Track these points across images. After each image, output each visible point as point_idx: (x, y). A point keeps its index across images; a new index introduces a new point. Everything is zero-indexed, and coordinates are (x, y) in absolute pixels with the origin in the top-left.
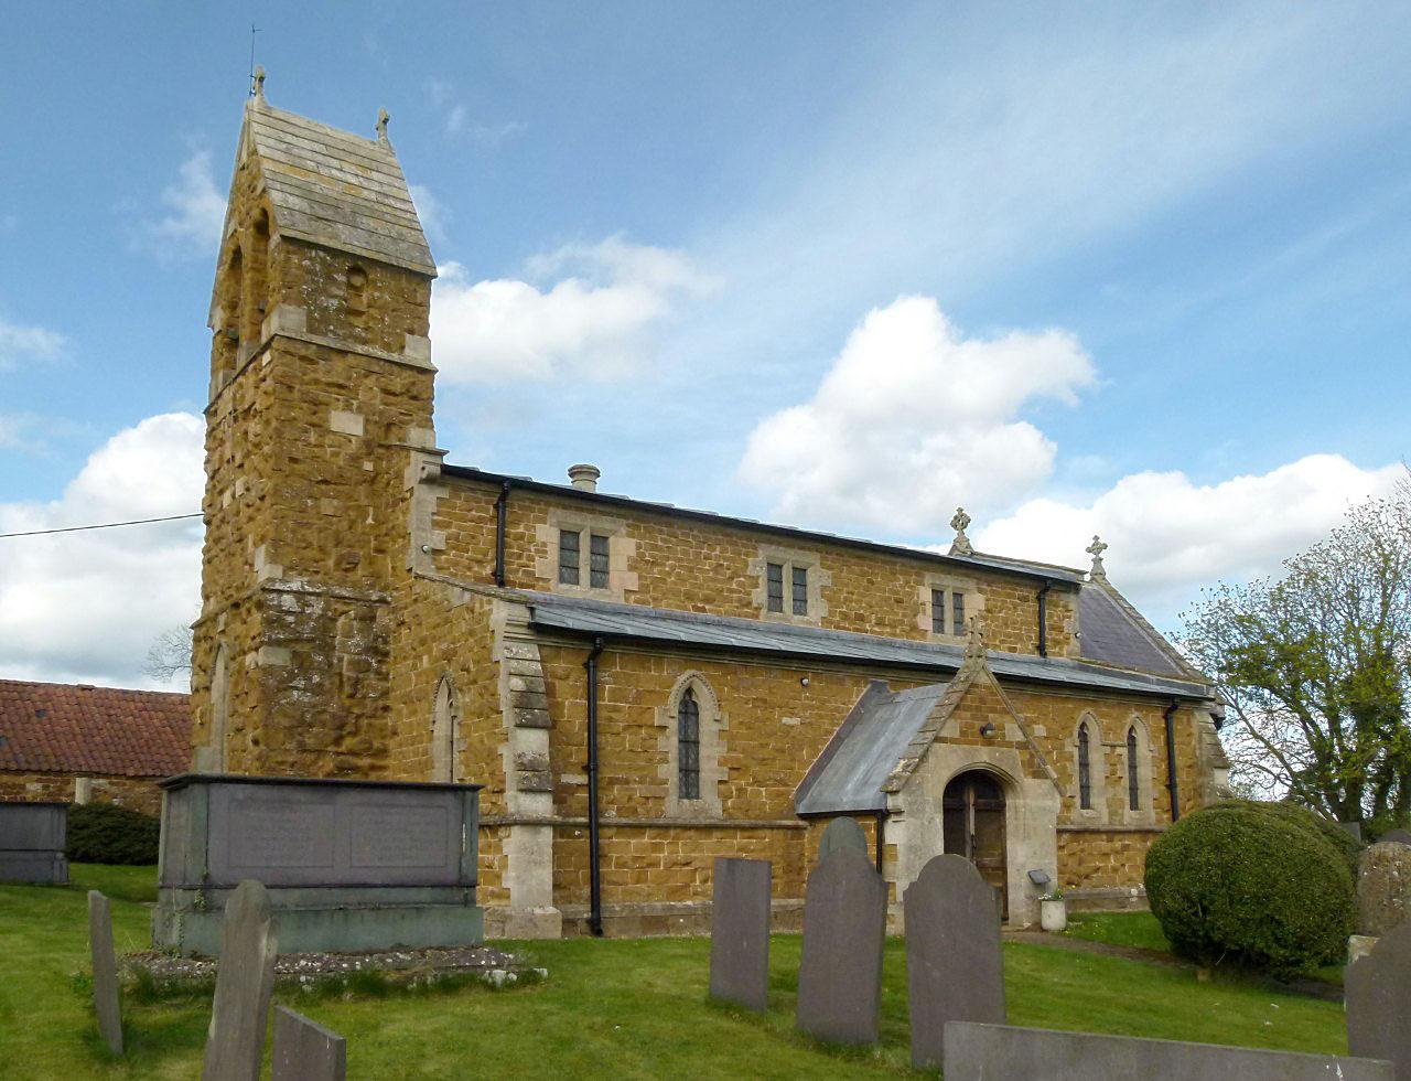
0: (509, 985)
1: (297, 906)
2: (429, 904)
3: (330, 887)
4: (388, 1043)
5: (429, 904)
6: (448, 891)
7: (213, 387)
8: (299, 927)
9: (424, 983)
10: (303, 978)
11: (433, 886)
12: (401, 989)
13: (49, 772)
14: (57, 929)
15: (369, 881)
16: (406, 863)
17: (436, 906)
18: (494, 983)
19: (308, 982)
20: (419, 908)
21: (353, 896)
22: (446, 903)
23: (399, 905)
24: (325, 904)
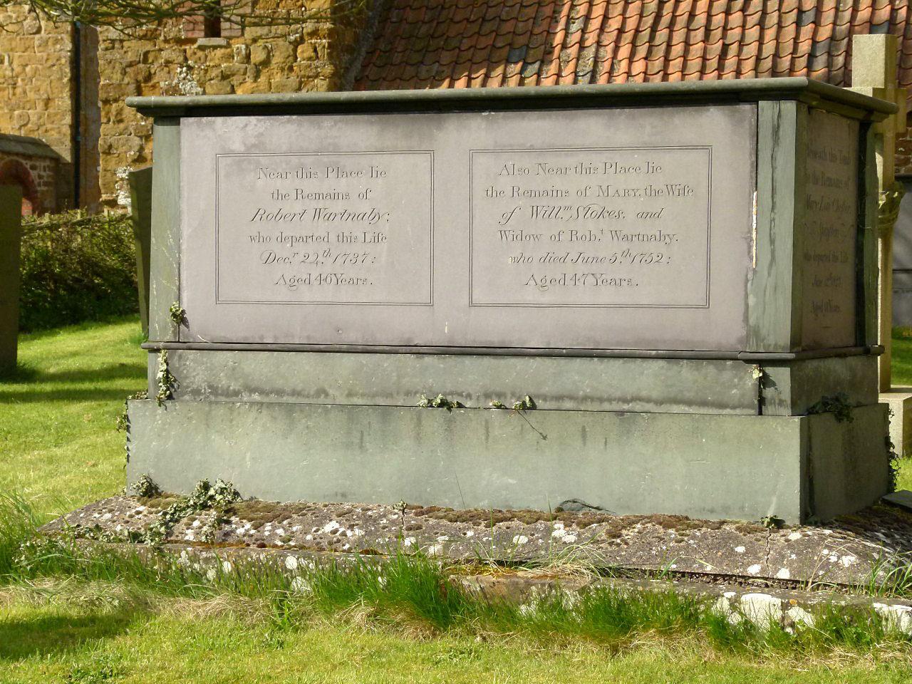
0: (786, 640)
1: (350, 395)
2: (659, 402)
3: (418, 351)
4: (47, 358)
5: (659, 402)
6: (710, 369)
7: (31, 150)
8: (348, 446)
9: (557, 607)
10: (291, 562)
11: (672, 357)
12: (500, 614)
13: (384, 20)
14: (7, 618)
15: (515, 341)
16: (607, 295)
17: (676, 409)
18: (747, 623)
19: (302, 571)
20: (625, 414)
21: (470, 376)
22: (704, 404)
23: (584, 401)
24: (408, 393)
